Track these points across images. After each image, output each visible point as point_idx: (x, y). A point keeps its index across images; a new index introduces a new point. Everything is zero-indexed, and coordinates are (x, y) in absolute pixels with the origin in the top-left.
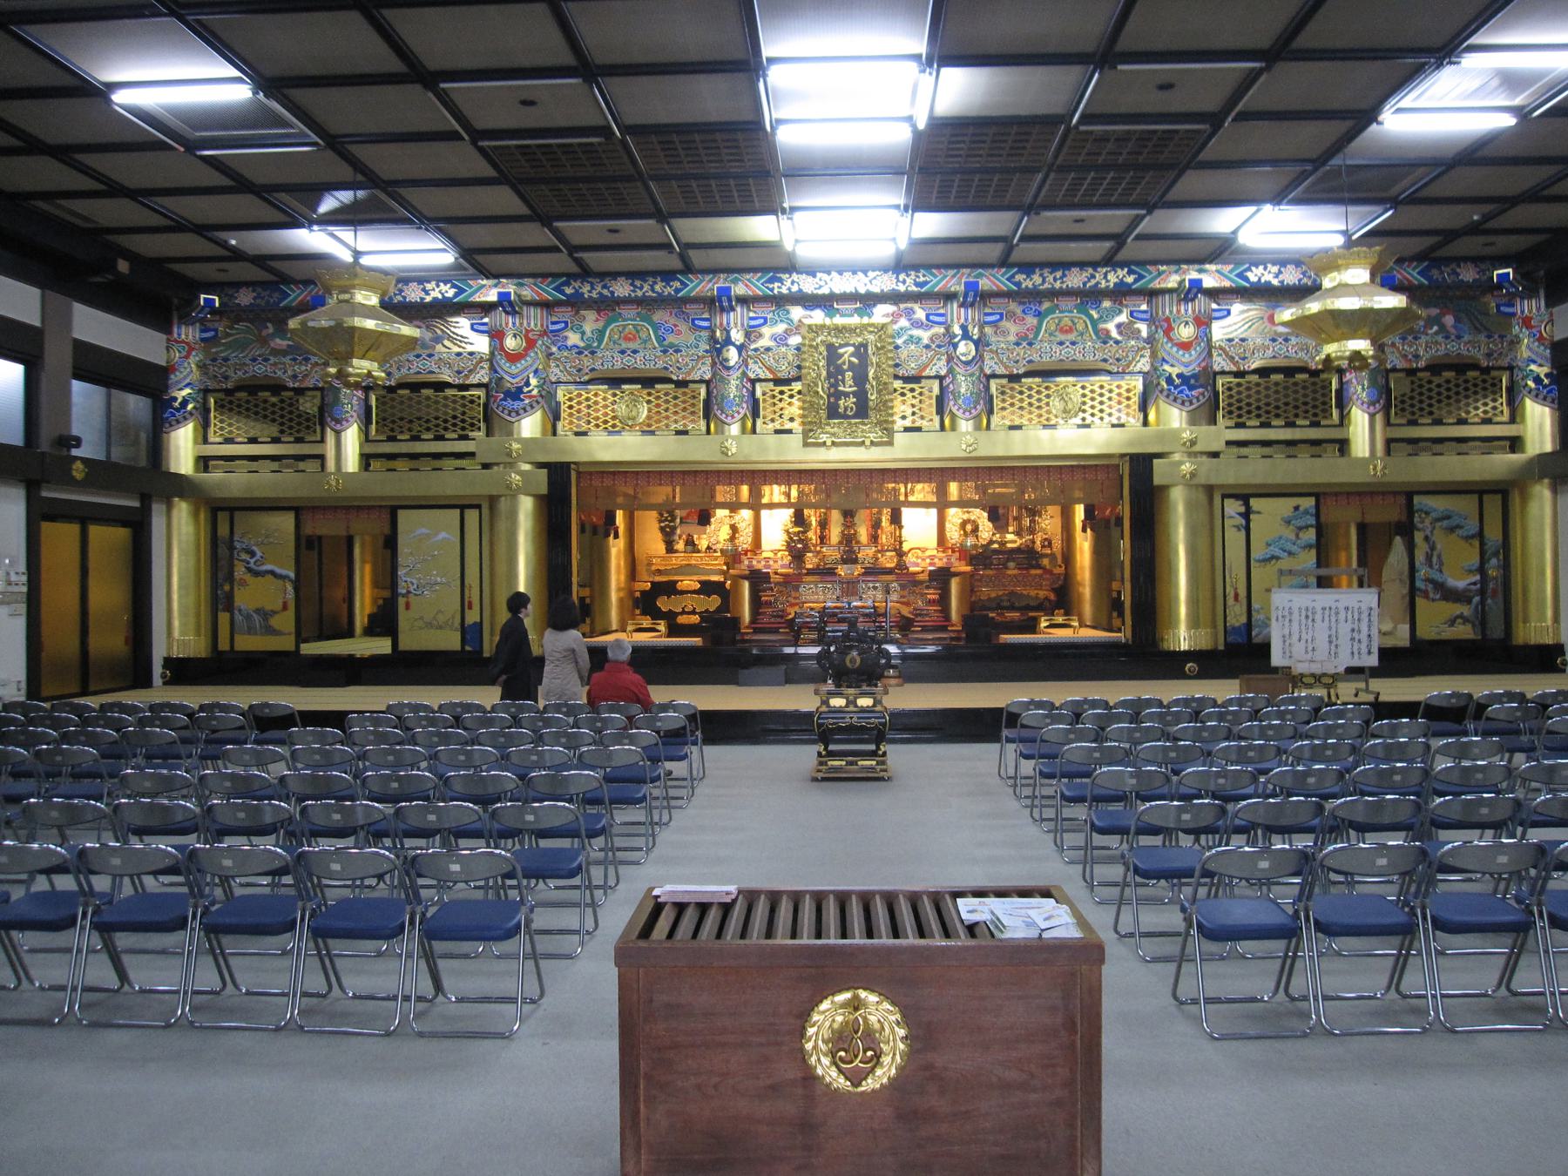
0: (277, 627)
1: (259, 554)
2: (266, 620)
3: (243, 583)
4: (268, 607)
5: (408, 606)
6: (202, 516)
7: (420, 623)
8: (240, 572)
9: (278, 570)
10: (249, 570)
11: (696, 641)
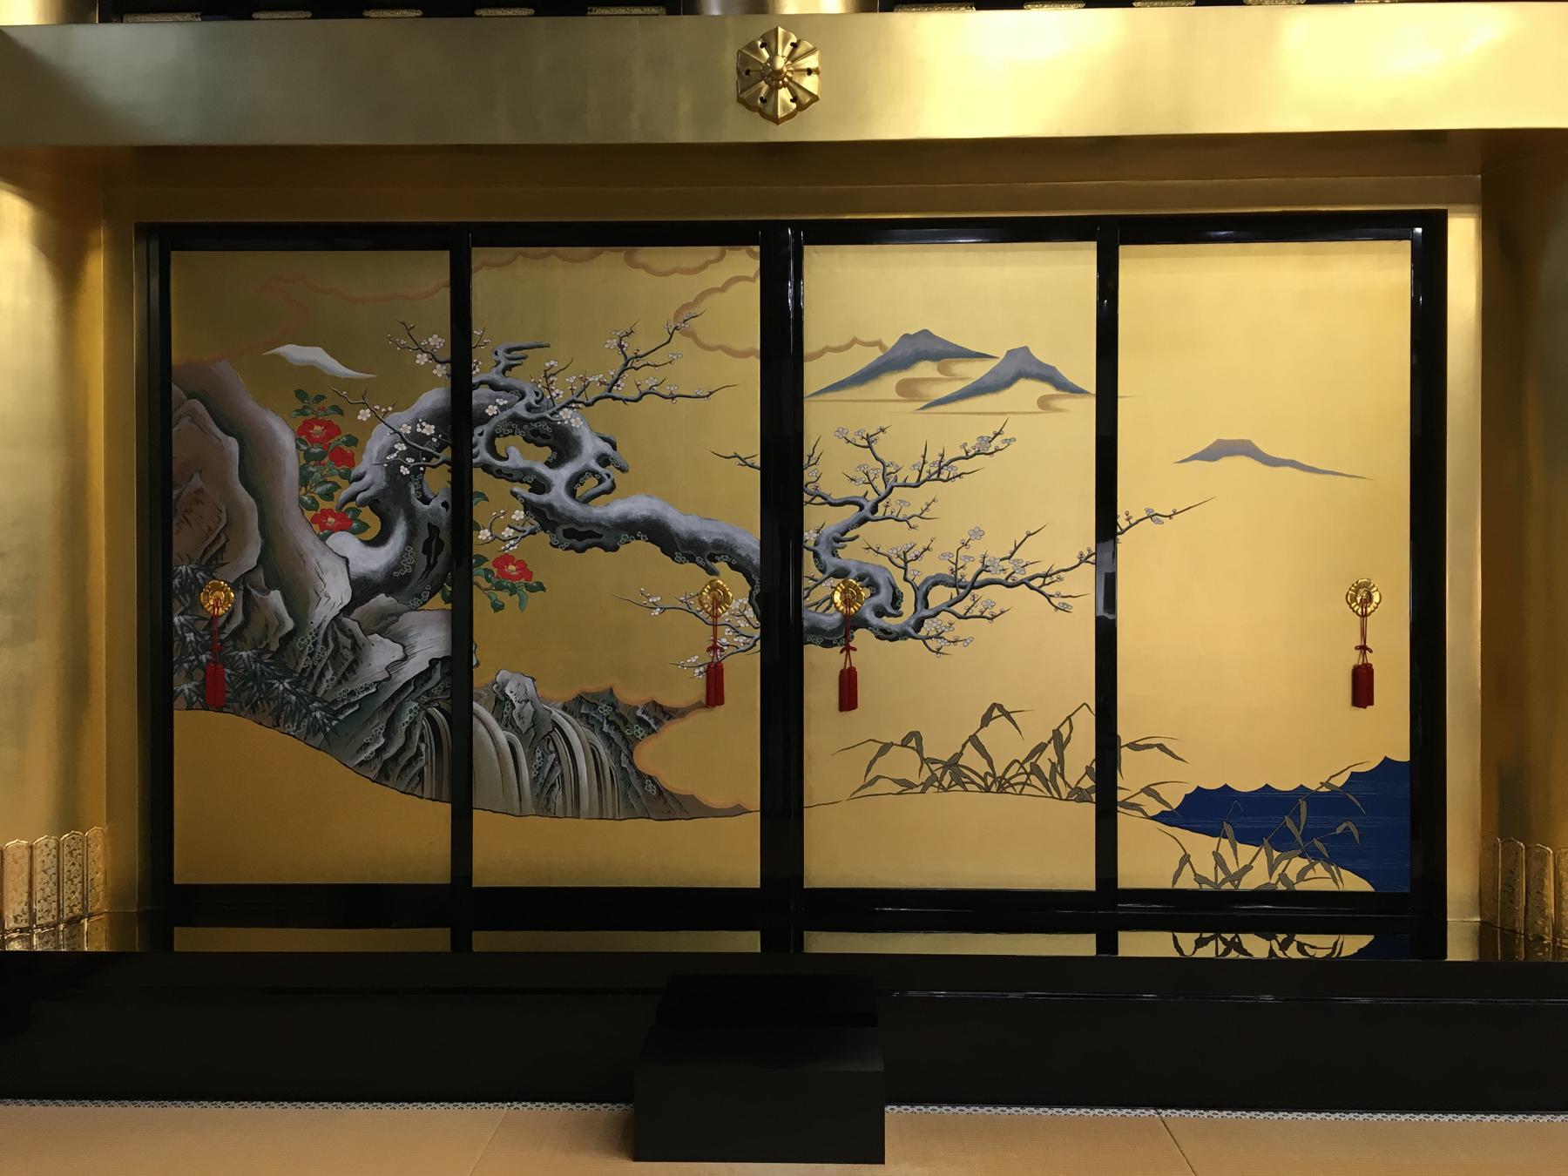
0: (674, 781)
1: (591, 446)
2: (624, 746)
3: (524, 581)
4: (632, 696)
5: (848, 696)
6: (96, 268)
7: (905, 764)
10: (545, 518)
11: (1353, 944)
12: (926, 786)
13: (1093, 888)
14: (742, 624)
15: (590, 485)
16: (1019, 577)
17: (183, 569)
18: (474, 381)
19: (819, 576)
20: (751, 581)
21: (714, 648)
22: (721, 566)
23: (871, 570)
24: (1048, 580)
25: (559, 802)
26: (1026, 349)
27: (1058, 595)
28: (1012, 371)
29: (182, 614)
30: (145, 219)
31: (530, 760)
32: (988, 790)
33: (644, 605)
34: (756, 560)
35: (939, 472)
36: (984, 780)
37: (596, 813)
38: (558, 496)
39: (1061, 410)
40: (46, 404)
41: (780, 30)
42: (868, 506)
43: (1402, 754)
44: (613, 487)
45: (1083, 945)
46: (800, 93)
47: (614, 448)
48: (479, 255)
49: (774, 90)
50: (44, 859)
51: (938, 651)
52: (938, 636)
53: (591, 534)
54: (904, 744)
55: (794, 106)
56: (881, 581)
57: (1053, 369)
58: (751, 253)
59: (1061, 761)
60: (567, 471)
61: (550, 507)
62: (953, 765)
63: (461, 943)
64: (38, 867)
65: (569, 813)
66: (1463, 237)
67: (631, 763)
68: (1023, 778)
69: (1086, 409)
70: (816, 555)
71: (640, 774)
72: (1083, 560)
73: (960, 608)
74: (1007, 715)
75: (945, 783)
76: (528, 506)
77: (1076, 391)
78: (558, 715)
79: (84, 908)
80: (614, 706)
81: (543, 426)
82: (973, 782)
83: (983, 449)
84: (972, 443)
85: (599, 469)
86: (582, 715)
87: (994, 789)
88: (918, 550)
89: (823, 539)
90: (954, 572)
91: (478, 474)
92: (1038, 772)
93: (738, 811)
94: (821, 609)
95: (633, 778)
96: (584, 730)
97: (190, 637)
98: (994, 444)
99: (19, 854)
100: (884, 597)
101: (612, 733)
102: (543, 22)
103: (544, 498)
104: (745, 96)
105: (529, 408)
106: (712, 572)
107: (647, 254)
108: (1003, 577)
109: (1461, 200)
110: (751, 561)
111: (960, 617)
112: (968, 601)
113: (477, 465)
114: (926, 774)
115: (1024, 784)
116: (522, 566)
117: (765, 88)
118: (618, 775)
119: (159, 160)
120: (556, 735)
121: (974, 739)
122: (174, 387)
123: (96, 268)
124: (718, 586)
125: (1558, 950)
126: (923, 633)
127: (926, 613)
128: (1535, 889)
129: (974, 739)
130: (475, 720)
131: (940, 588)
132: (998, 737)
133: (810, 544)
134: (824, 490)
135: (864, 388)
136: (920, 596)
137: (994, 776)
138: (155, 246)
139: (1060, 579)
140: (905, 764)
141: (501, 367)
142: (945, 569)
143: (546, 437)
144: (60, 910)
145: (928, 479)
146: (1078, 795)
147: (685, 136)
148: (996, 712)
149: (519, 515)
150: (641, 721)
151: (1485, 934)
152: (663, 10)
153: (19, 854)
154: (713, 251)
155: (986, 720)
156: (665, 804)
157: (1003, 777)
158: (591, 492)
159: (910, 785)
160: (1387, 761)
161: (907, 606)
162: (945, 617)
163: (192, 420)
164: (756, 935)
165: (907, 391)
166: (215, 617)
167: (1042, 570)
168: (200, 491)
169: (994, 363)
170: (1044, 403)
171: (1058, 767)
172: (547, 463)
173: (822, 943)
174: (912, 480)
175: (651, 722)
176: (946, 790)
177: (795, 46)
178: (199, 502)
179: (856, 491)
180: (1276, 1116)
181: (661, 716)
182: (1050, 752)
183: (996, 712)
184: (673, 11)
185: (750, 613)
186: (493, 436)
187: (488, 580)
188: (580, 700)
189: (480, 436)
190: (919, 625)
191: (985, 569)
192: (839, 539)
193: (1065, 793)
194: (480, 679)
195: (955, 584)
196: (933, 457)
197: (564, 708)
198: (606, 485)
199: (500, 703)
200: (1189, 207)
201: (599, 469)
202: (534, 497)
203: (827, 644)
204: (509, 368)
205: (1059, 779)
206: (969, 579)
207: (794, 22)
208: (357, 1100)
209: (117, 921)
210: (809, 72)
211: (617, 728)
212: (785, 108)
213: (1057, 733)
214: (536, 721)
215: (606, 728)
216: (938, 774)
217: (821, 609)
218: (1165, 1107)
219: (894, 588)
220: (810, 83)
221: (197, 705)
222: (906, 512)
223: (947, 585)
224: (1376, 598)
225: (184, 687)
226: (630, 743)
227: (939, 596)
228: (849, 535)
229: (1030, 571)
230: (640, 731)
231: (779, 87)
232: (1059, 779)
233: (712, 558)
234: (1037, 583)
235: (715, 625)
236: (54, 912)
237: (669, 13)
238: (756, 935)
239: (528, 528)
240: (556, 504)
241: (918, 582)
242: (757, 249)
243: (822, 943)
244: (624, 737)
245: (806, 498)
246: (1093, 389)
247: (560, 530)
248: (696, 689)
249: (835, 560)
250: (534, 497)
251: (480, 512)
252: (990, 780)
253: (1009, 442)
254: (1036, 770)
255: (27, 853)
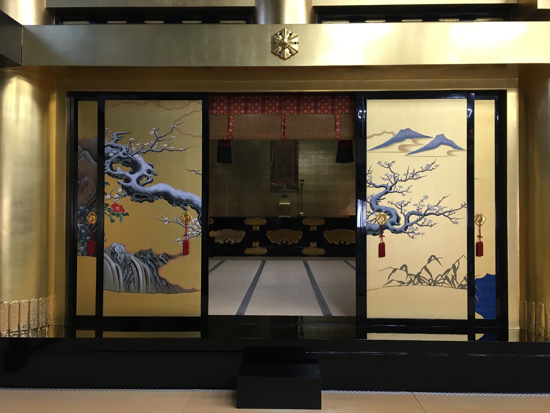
0: (172, 280)
1: (145, 167)
2: (155, 268)
4: (158, 251)
5: (382, 252)
6: (53, 107)
7: (401, 275)
8: (113, 192)
9: (175, 193)
10: (129, 191)
12: (409, 283)
13: (200, 316)
14: (196, 227)
15: (144, 181)
16: (441, 212)
17: (81, 208)
18: (106, 144)
19: (372, 211)
20: (198, 213)
21: (186, 235)
22: (188, 208)
23: (389, 209)
24: (451, 213)
25: (133, 287)
26: (443, 135)
27: (454, 218)
28: (438, 143)
29: (80, 223)
30: (73, 92)
31: (123, 273)
32: (430, 285)
33: (162, 221)
34: (200, 205)
35: (413, 176)
36: (429, 281)
37: (145, 291)
38: (133, 184)
39: (455, 155)
40: (36, 153)
41: (286, 30)
42: (388, 188)
43: (493, 272)
44: (152, 181)
45: (464, 338)
46: (292, 50)
47: (153, 167)
48: (108, 103)
49: (283, 49)
50: (33, 306)
51: (413, 237)
52: (413, 232)
53: (145, 197)
54: (401, 269)
55: (290, 54)
56: (393, 213)
57: (452, 141)
58: (199, 102)
59: (455, 275)
60: (137, 175)
61: (131, 187)
62: (418, 276)
63: (99, 334)
64: (31, 309)
65: (136, 291)
66: (512, 98)
67: (157, 274)
68: (442, 281)
69: (464, 154)
70: (371, 204)
71: (161, 279)
72: (463, 206)
73: (420, 223)
74: (437, 259)
75: (415, 282)
76: (123, 187)
77: (460, 149)
78: (133, 258)
79: (46, 323)
80: (152, 255)
81: (129, 160)
82: (425, 282)
83: (428, 168)
84: (424, 166)
85: (148, 175)
86: (141, 258)
87: (432, 284)
88: (406, 202)
89: (373, 199)
90: (418, 210)
91: (106, 175)
92: (448, 279)
93: (194, 290)
94: (372, 223)
95: (158, 279)
96: (142, 263)
97: (83, 231)
98: (432, 167)
99: (25, 304)
100: (394, 219)
101: (151, 264)
102: (206, 27)
103: (129, 184)
104: (274, 51)
105: (124, 154)
106: (185, 209)
107: (163, 103)
108: (435, 212)
109: (511, 87)
110: (198, 206)
111: (420, 226)
112: (423, 220)
113: (106, 173)
114: (409, 279)
115: (443, 283)
116: (121, 207)
117: (280, 48)
118: (153, 278)
119: (75, 71)
120: (132, 265)
121: (425, 267)
122: (79, 147)
123: (53, 107)
124: (187, 214)
125: (546, 338)
126: (407, 231)
127: (408, 224)
128: (538, 318)
129: (425, 267)
130: (104, 259)
131: (413, 216)
132: (434, 267)
133: (369, 200)
134: (373, 182)
135: (387, 148)
136: (407, 218)
137: (432, 280)
138: (73, 99)
139: (455, 213)
140: (401, 275)
141: (114, 140)
142: (415, 209)
143: (129, 164)
144: (38, 324)
145: (409, 179)
146: (461, 287)
147: (254, 64)
148: (433, 258)
149: (120, 190)
150: (161, 260)
151: (522, 332)
152: (245, 22)
153: (25, 304)
154: (187, 102)
155: (430, 261)
156: (169, 288)
157: (435, 280)
158: (145, 182)
159: (403, 283)
160: (488, 275)
161: (402, 222)
162: (415, 226)
163: (85, 158)
164: (200, 332)
165: (402, 149)
166: (91, 225)
167: (448, 210)
168: (87, 182)
169: (431, 140)
170: (449, 153)
171: (454, 277)
172: (130, 173)
173: (372, 336)
174: (404, 179)
175: (164, 260)
176: (415, 285)
177: (291, 34)
178: (86, 185)
179: (385, 183)
180: (452, 394)
181: (168, 258)
182: (452, 272)
183: (433, 258)
184: (248, 23)
185: (198, 223)
186: (112, 163)
187: (110, 212)
188: (140, 252)
189: (107, 163)
190: (406, 228)
191: (428, 209)
192: (378, 198)
193: (457, 286)
194: (106, 245)
195: (419, 214)
196: (411, 171)
197: (135, 256)
198: (150, 180)
199: (113, 254)
200: (267, 89)
201: (148, 175)
202: (125, 184)
203: (375, 235)
204: (117, 140)
205: (455, 281)
206: (423, 212)
207: (290, 26)
208: (118, 388)
209: (57, 328)
210: (295, 43)
211: (153, 262)
212: (287, 55)
213: (454, 266)
214: (125, 261)
215: (149, 262)
216: (413, 279)
217: (372, 223)
218: (415, 391)
219: (398, 215)
220: (295, 47)
221: (85, 254)
222: (402, 190)
223: (416, 215)
224: (484, 219)
225: (81, 248)
226: (157, 267)
227: (413, 218)
228: (382, 198)
229: (444, 210)
230: (160, 263)
231: (285, 48)
232: (455, 281)
233: (185, 205)
234: (447, 214)
235: (186, 228)
236: (36, 325)
237: (247, 23)
238: (200, 332)
239: (123, 194)
240: (133, 186)
241: (406, 214)
242: (201, 101)
243: (372, 336)
244: (155, 265)
245: (368, 185)
246: (466, 149)
247: (134, 195)
248: (180, 249)
249: (377, 206)
250: (125, 184)
251: (107, 189)
252: (431, 281)
253: (437, 166)
254: (447, 278)
255: (28, 304)
